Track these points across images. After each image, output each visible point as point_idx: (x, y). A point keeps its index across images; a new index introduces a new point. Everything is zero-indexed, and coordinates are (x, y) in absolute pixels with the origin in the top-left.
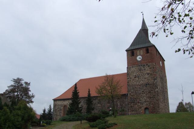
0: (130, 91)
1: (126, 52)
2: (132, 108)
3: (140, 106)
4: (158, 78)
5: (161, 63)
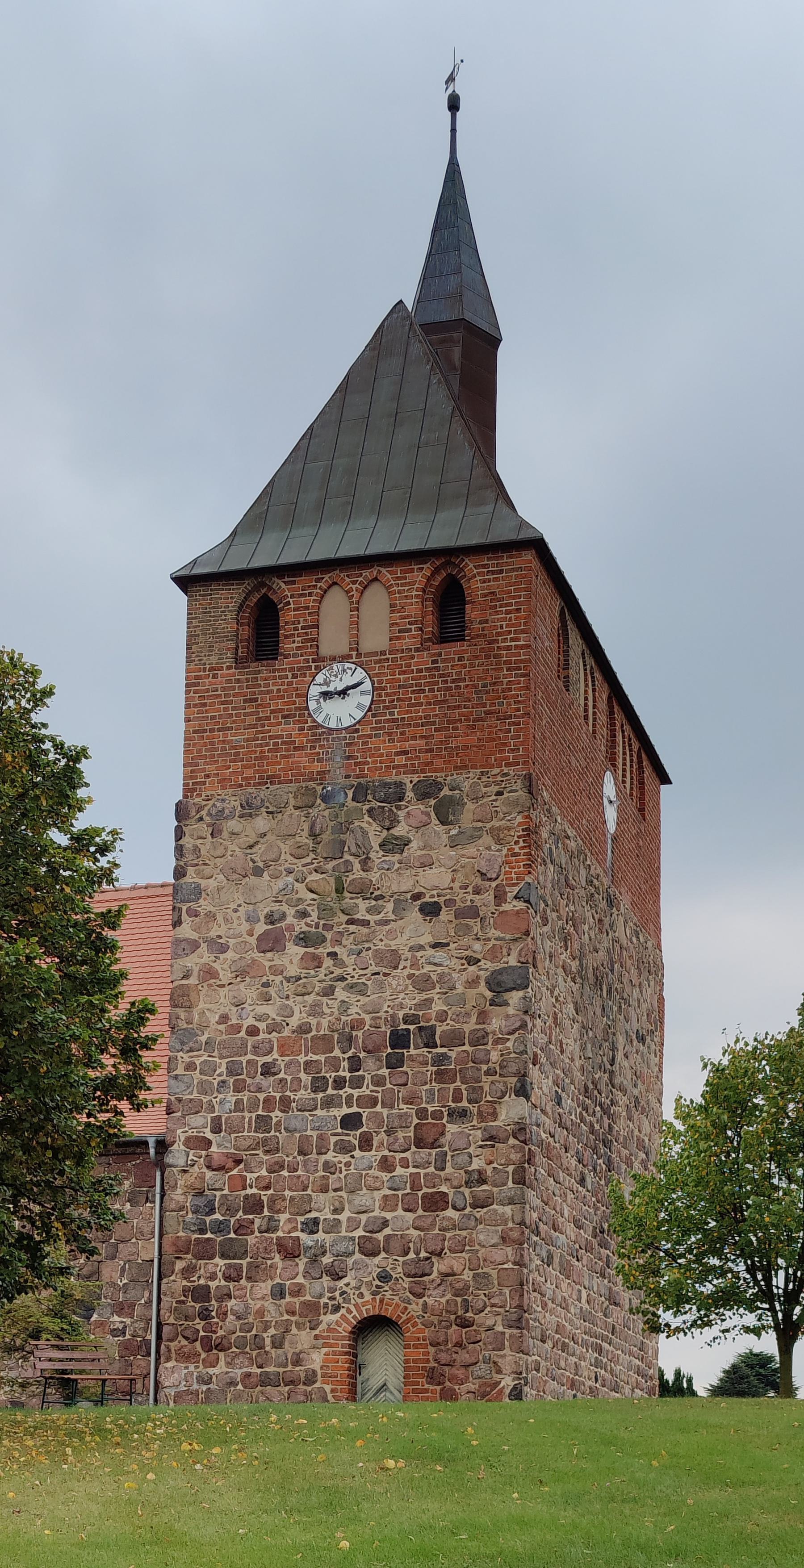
0: (196, 1108)
1: (180, 598)
2: (205, 1315)
3: (298, 1291)
4: (545, 964)
5: (609, 789)
